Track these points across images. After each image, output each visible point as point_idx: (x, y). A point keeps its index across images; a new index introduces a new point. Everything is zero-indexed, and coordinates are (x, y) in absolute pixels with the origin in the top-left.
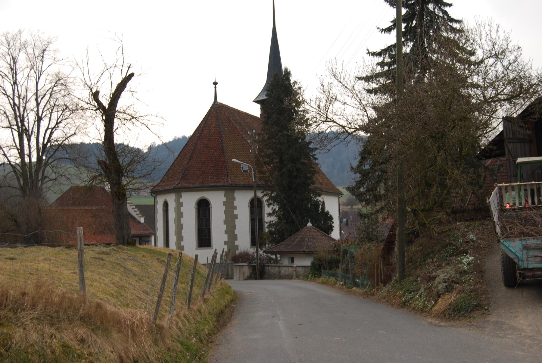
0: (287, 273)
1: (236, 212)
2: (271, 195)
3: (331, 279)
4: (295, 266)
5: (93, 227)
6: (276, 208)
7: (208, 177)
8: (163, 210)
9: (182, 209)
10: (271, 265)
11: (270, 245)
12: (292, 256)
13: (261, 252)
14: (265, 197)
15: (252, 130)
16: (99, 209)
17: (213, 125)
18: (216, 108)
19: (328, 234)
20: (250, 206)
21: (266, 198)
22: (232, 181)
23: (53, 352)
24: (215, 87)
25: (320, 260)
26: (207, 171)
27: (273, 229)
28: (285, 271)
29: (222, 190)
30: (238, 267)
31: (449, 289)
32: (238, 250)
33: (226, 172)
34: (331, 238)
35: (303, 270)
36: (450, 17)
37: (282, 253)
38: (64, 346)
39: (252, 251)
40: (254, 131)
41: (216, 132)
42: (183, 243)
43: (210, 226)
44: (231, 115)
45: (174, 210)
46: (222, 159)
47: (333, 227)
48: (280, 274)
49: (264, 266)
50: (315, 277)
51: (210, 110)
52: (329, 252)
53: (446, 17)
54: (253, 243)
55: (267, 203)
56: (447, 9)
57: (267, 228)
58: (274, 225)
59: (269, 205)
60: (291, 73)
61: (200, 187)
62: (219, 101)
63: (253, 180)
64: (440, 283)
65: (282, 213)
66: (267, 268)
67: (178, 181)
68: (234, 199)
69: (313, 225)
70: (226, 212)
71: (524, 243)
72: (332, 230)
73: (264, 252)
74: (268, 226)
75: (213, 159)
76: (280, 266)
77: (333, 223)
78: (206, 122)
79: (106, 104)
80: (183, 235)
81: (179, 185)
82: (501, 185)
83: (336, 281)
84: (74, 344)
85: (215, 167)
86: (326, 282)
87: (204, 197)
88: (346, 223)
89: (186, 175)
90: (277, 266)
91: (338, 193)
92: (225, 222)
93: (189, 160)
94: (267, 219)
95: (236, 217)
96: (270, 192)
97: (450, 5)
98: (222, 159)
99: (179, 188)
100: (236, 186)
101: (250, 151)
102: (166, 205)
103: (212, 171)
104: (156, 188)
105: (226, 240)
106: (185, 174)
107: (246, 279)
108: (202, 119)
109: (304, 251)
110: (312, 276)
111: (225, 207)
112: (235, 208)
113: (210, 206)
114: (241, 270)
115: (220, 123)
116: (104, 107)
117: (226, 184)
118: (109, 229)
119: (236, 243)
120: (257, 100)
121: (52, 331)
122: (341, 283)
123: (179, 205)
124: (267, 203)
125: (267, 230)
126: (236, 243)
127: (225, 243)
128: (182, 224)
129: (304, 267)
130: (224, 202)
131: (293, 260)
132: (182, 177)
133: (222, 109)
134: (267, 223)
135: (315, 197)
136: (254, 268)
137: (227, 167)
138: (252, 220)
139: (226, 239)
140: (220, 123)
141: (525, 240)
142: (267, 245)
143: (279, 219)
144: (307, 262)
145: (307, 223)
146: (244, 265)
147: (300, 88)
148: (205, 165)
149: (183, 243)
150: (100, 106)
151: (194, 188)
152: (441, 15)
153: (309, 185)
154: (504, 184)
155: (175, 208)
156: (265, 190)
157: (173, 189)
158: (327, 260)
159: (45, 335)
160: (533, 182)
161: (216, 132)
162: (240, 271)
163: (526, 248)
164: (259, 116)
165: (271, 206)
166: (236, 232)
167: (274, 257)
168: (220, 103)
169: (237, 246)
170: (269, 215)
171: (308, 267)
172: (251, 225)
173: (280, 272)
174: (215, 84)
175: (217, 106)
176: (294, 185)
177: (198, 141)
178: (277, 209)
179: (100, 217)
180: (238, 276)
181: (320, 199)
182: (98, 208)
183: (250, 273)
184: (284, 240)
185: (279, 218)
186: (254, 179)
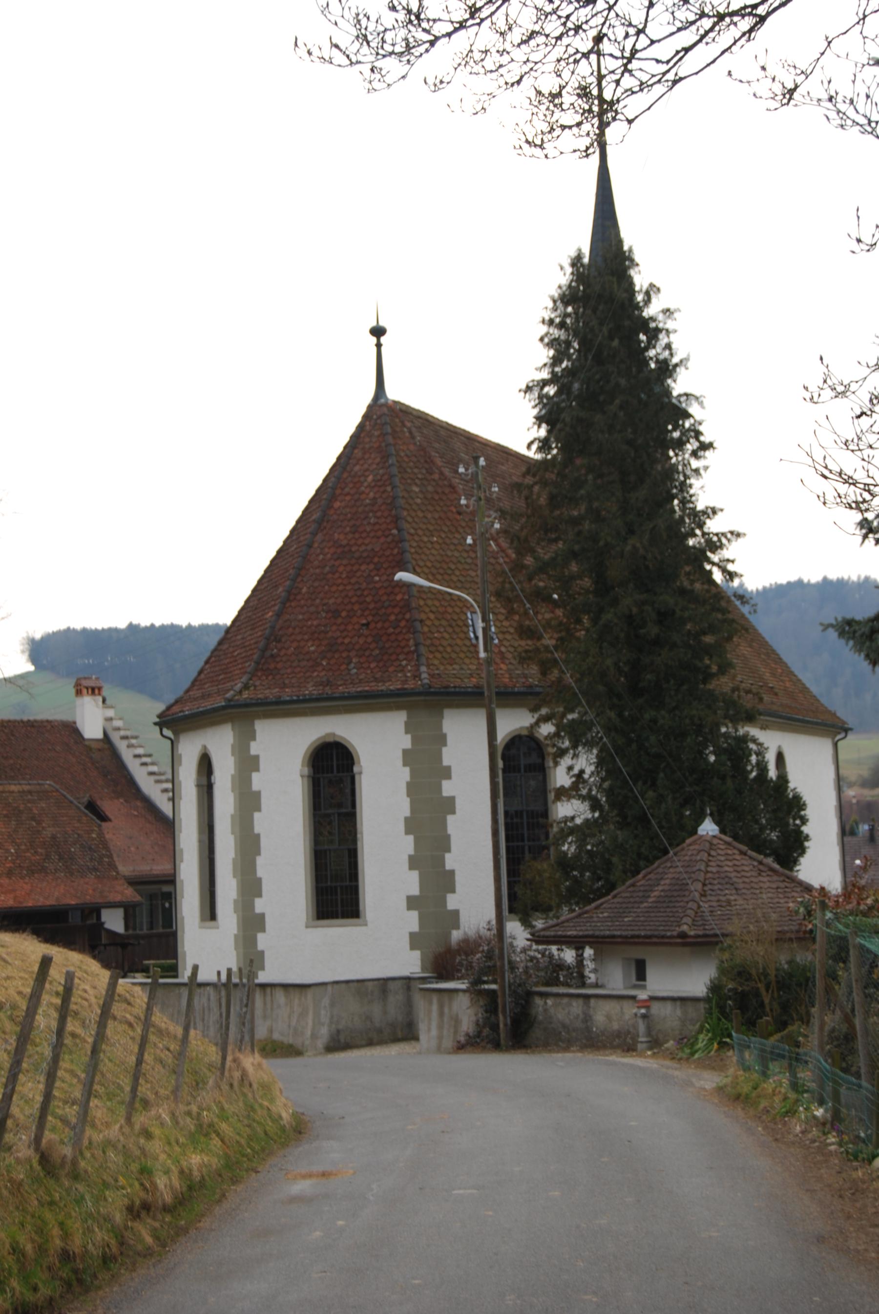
0: (615, 1026)
1: (448, 788)
3: (769, 1086)
5: (7, 851)
7: (350, 662)
8: (199, 786)
9: (257, 781)
12: (638, 953)
15: (476, 459)
16: (30, 792)
17: (370, 478)
18: (379, 417)
19: (791, 870)
22: (432, 676)
24: (379, 346)
25: (742, 973)
26: (347, 641)
28: (608, 1017)
29: (398, 707)
30: (435, 998)
32: (457, 927)
33: (411, 642)
35: (679, 1012)
40: (482, 462)
41: (380, 501)
42: (260, 906)
43: (355, 841)
44: (437, 445)
45: (229, 785)
46: (399, 597)
47: (807, 838)
48: (588, 1029)
49: (530, 994)
50: (722, 1045)
51: (361, 427)
52: (780, 939)
61: (317, 700)
62: (393, 393)
63: (482, 655)
66: (538, 1001)
67: (244, 679)
68: (442, 740)
69: (723, 831)
70: (412, 789)
72: (803, 851)
75: (368, 599)
76: (587, 997)
77: (804, 820)
78: (344, 469)
80: (260, 873)
81: (245, 695)
83: (792, 1096)
85: (372, 626)
86: (747, 1097)
87: (334, 735)
88: (867, 834)
89: (272, 656)
90: (578, 996)
91: (833, 726)
92: (411, 826)
93: (283, 603)
95: (449, 805)
96: (561, 709)
98: (399, 597)
99: (246, 706)
100: (448, 694)
101: (469, 540)
102: (206, 765)
103: (361, 641)
104: (176, 709)
105: (415, 891)
106: (268, 653)
107: (461, 1048)
108: (334, 460)
109: (683, 935)
110: (711, 1040)
112: (447, 773)
113: (356, 769)
114: (446, 1010)
115: (395, 470)
117: (410, 685)
118: (61, 858)
119: (452, 902)
122: (819, 1112)
126: (452, 902)
127: (412, 903)
128: (258, 836)
129: (683, 1000)
130: (405, 752)
131: (641, 975)
132: (257, 663)
133: (402, 422)
137: (418, 624)
139: (415, 890)
140: (395, 470)
145: (699, 821)
146: (456, 991)
147: (667, 312)
148: (339, 621)
149: (260, 906)
151: (298, 701)
153: (708, 677)
155: (233, 776)
157: (224, 708)
158: (772, 973)
161: (380, 501)
162: (441, 1014)
166: (450, 861)
167: (569, 956)
169: (456, 913)
171: (695, 1000)
173: (587, 1018)
174: (378, 332)
175: (385, 410)
176: (649, 677)
177: (314, 534)
178: (589, 770)
179: (33, 818)
180: (434, 1032)
181: (711, 686)
182: (26, 788)
183: (477, 1024)
184: (611, 887)
186: (486, 650)
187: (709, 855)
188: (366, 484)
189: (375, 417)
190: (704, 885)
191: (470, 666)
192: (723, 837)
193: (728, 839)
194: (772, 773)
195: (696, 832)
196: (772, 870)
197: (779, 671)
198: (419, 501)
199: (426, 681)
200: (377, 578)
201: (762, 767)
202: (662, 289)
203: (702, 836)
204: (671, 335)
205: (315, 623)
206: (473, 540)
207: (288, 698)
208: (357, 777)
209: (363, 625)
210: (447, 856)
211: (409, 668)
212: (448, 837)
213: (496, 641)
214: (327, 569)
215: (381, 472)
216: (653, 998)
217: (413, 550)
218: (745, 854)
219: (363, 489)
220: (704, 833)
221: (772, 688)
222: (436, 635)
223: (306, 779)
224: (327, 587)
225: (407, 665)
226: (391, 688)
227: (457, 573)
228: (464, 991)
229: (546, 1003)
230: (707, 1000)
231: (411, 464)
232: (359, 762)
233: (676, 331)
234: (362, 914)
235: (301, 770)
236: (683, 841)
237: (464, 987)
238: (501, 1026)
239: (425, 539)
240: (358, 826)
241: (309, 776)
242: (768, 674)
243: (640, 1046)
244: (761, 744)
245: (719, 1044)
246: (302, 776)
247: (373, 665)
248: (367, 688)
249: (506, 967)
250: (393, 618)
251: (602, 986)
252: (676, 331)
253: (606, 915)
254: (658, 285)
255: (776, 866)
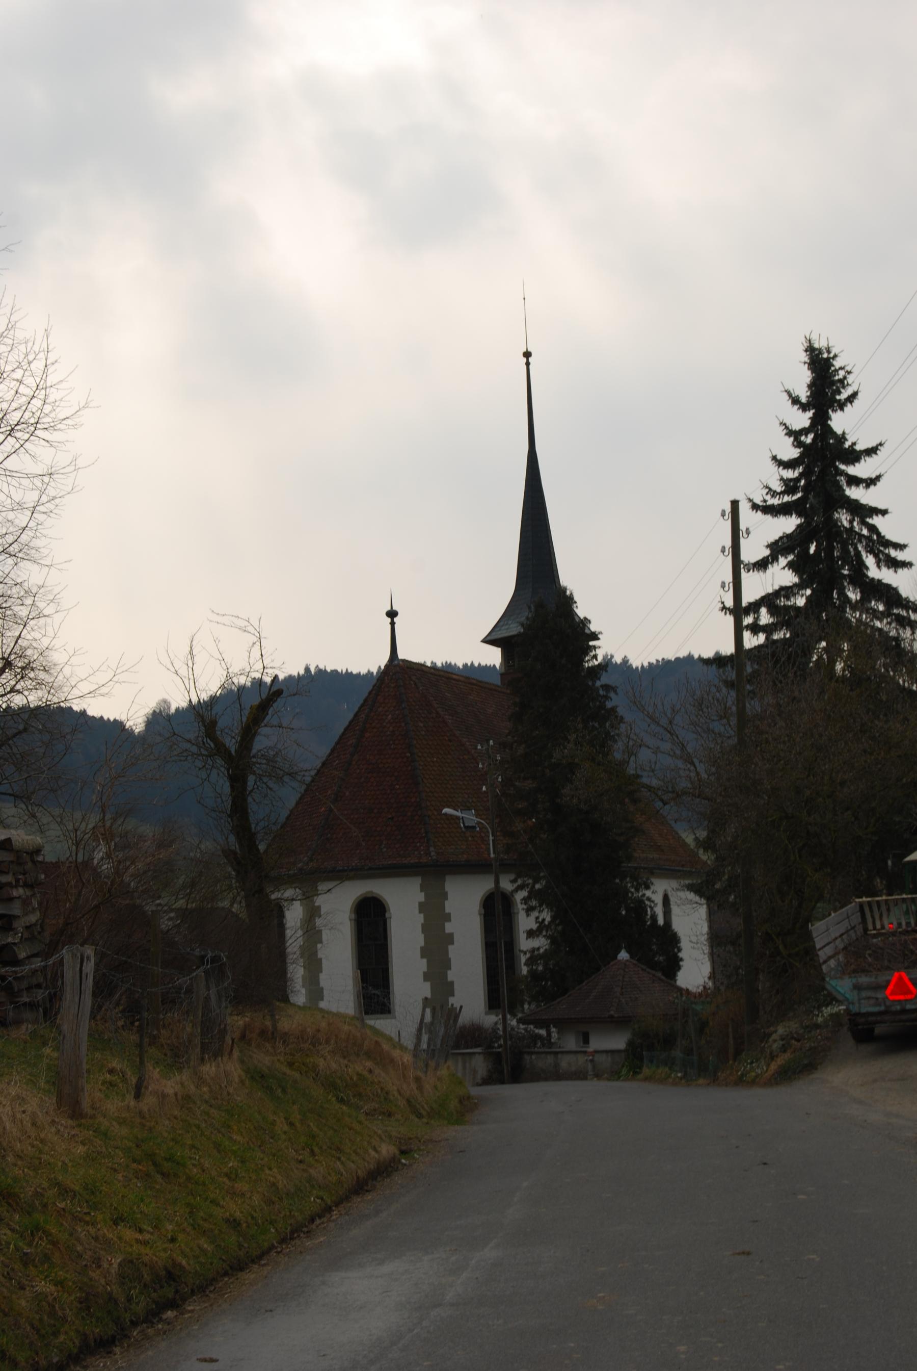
1: (449, 928)
2: (533, 886)
4: (591, 1050)
6: (547, 916)
10: (536, 1050)
11: (533, 1006)
13: (514, 1023)
14: (519, 892)
15: (488, 741)
20: (483, 912)
21: (523, 894)
23: (351, 1079)
24: (393, 624)
26: (378, 829)
27: (540, 968)
29: (415, 874)
31: (784, 1049)
33: (423, 830)
34: (680, 990)
36: (884, 537)
37: (563, 1024)
38: (358, 1074)
39: (491, 1020)
40: (491, 742)
46: (413, 800)
47: (681, 960)
53: (875, 537)
54: (493, 1002)
55: (525, 907)
56: (876, 521)
57: (525, 964)
58: (541, 957)
59: (529, 910)
60: (576, 599)
62: (402, 655)
64: (775, 1041)
65: (560, 928)
66: (527, 1057)
68: (445, 896)
69: (632, 957)
70: (425, 929)
71: (854, 980)
72: (679, 968)
73: (520, 1021)
74: (527, 960)
76: (556, 1053)
79: (232, 745)
80: (322, 983)
82: (860, 900)
84: (365, 1073)
90: (550, 1053)
92: (424, 952)
94: (525, 944)
95: (450, 938)
97: (884, 512)
98: (413, 800)
109: (612, 1017)
111: (422, 915)
113: (387, 915)
116: (227, 751)
120: (489, 638)
121: (346, 1062)
122: (679, 1075)
123: (313, 913)
124: (525, 907)
125: (525, 970)
129: (612, 1052)
130: (420, 904)
131: (586, 1041)
134: (525, 953)
135: (637, 890)
136: (497, 1059)
138: (490, 947)
141: (855, 977)
142: (526, 1006)
143: (552, 943)
144: (618, 1042)
146: (474, 1053)
150: (220, 749)
152: (865, 532)
154: (864, 899)
156: (519, 876)
159: (342, 1065)
160: (904, 896)
162: (464, 1068)
163: (857, 987)
164: (499, 683)
165: (535, 914)
166: (451, 975)
167: (543, 1032)
168: (404, 661)
170: (531, 934)
171: (619, 1051)
172: (487, 958)
174: (392, 614)
178: (548, 919)
185: (553, 940)
186: (494, 853)
187: (624, 971)
188: (387, 721)
189: (391, 674)
190: (622, 988)
191: (462, 846)
192: (632, 960)
193: (635, 962)
194: (661, 921)
195: (616, 958)
196: (660, 979)
197: (665, 831)
198: (423, 733)
199: (434, 857)
200: (398, 787)
201: (654, 918)
202: (591, 621)
203: (620, 961)
204: (597, 650)
205: (356, 816)
206: (487, 789)
207: (341, 868)
208: (388, 920)
209: (389, 818)
210: (449, 972)
211: (422, 848)
212: (449, 960)
213: (478, 829)
214: (363, 779)
215: (397, 712)
216: (596, 1052)
217: (421, 768)
218: (645, 970)
219: (385, 724)
220: (621, 958)
221: (660, 846)
222: (439, 826)
223: (353, 922)
224: (363, 792)
225: (420, 846)
226: (412, 861)
227: (451, 782)
228: (479, 1053)
229: (531, 1058)
230: (626, 1051)
231: (417, 707)
232: (389, 910)
233: (600, 647)
234: (392, 1011)
235: (349, 916)
236: (609, 963)
237: (480, 1051)
238: (505, 1071)
239: (429, 760)
240: (389, 953)
241: (355, 920)
242: (656, 835)
243: (589, 1077)
244: (653, 902)
245: (633, 1072)
246: (351, 920)
247: (397, 846)
248: (395, 862)
249: (508, 1037)
250: (409, 814)
251: (563, 1048)
252: (600, 647)
253: (564, 1006)
254: (589, 618)
255: (663, 978)
